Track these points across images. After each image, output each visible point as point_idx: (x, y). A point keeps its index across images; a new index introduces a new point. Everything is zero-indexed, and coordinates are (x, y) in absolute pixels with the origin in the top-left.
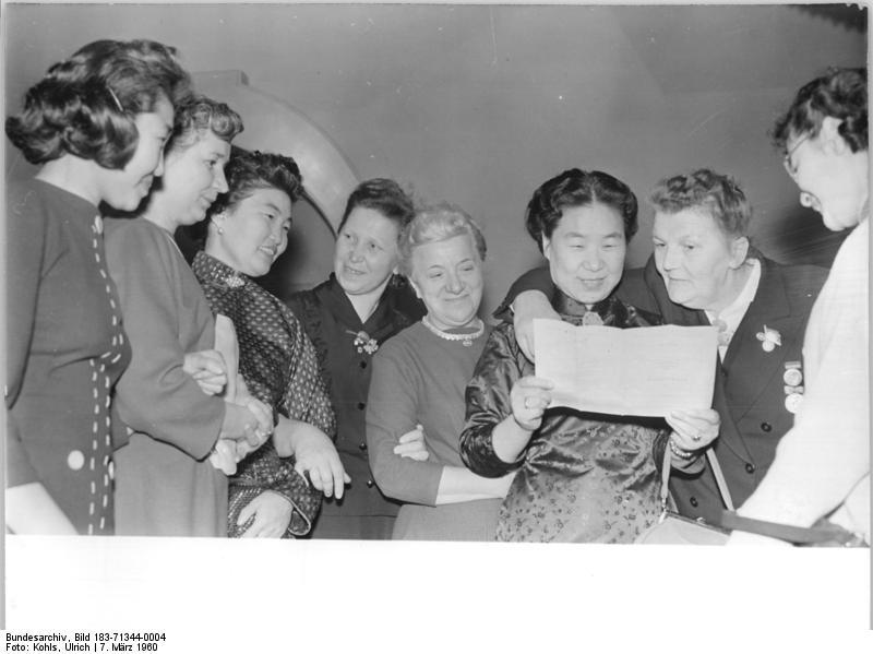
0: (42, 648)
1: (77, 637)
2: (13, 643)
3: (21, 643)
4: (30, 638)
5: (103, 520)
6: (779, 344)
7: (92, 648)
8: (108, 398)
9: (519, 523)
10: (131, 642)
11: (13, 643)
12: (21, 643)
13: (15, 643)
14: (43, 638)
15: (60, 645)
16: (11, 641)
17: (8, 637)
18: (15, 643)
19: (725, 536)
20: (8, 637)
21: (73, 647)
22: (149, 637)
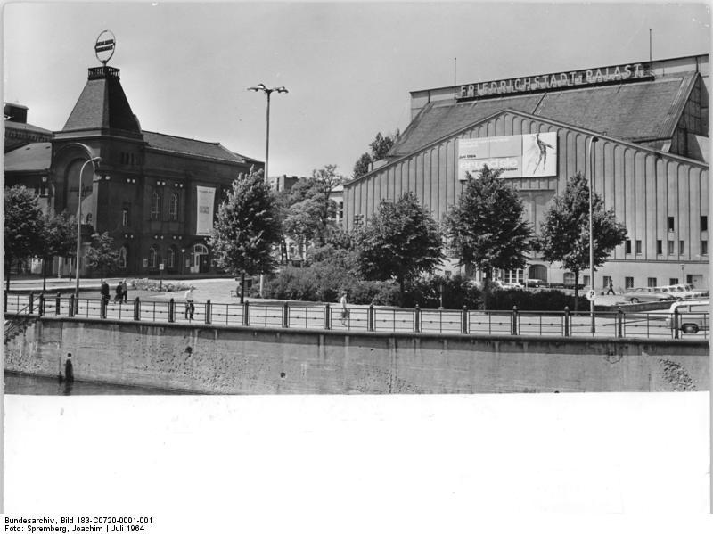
0: (33, 530)
1: (63, 520)
2: (11, 525)
3: (17, 525)
4: (25, 521)
5: (93, 236)
6: (699, 138)
7: (105, 529)
8: (700, 293)
9: (319, 277)
10: (60, 525)
11: (11, 525)
12: (17, 525)
13: (12, 525)
14: (35, 521)
15: (70, 527)
16: (9, 524)
17: (7, 520)
18: (12, 525)
19: (701, 359)
20: (7, 520)
21: (77, 529)
22: (123, 520)
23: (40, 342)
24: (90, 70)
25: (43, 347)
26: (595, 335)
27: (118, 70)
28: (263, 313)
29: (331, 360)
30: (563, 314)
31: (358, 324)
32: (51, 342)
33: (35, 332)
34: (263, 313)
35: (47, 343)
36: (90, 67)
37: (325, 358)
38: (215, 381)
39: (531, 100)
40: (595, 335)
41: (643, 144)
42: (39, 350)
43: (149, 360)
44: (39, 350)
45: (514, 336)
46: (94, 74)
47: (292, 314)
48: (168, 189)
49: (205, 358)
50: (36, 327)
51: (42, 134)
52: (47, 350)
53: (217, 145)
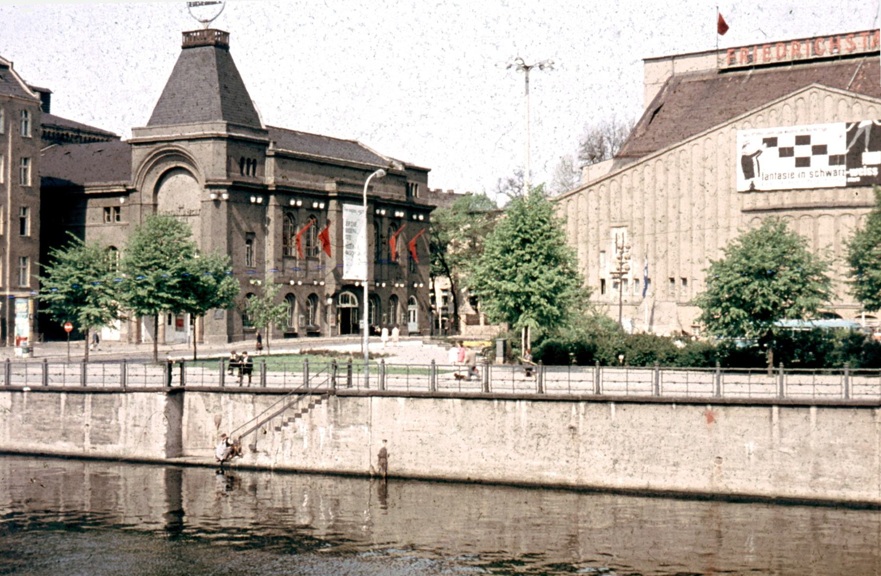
23: (337, 425)
24: (184, 34)
25: (342, 433)
26: (350, 389)
27: (226, 34)
28: (93, 370)
29: (790, 439)
30: (843, 373)
31: (638, 386)
32: (354, 424)
33: (329, 411)
34: (572, 384)
35: (348, 426)
36: (186, 30)
37: (782, 437)
38: (614, 470)
39: (766, 80)
40: (350, 389)
41: (182, 142)
42: (335, 436)
43: (510, 445)
44: (335, 436)
45: (541, 395)
46: (191, 42)
47: (130, 372)
48: (304, 210)
49: (597, 440)
50: (328, 404)
51: (78, 131)
52: (348, 435)
53: (355, 143)
